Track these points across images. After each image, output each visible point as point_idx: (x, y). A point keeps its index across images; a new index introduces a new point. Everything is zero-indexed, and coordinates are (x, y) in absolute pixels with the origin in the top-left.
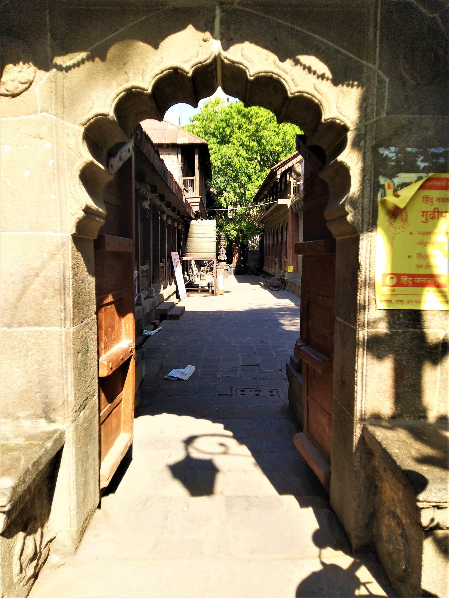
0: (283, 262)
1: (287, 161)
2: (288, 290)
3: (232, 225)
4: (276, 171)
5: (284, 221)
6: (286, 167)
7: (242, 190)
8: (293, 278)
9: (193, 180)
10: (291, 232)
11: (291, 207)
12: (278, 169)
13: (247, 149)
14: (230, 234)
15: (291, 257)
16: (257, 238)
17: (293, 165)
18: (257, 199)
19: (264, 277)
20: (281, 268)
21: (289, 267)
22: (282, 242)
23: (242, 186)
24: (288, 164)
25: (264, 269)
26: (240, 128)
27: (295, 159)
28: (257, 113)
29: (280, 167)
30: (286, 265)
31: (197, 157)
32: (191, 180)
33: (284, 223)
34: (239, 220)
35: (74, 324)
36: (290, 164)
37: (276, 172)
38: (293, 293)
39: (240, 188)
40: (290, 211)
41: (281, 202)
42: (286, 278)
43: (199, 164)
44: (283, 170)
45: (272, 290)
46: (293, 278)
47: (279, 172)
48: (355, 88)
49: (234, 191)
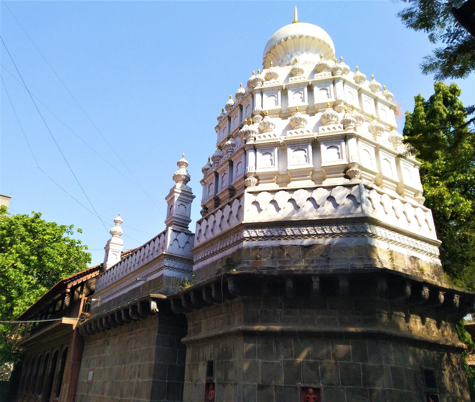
5: (62, 346)
6: (80, 281)
7: (9, 305)
10: (71, 360)
11: (77, 328)
12: (69, 282)
13: (27, 262)
15: (67, 395)
16: (11, 366)
18: (26, 316)
22: (30, 375)
24: (81, 279)
26: (23, 239)
27: (90, 275)
28: (44, 230)
29: (72, 280)
33: (62, 348)
36: (84, 279)
41: (66, 320)
44: (75, 283)
47: (69, 286)
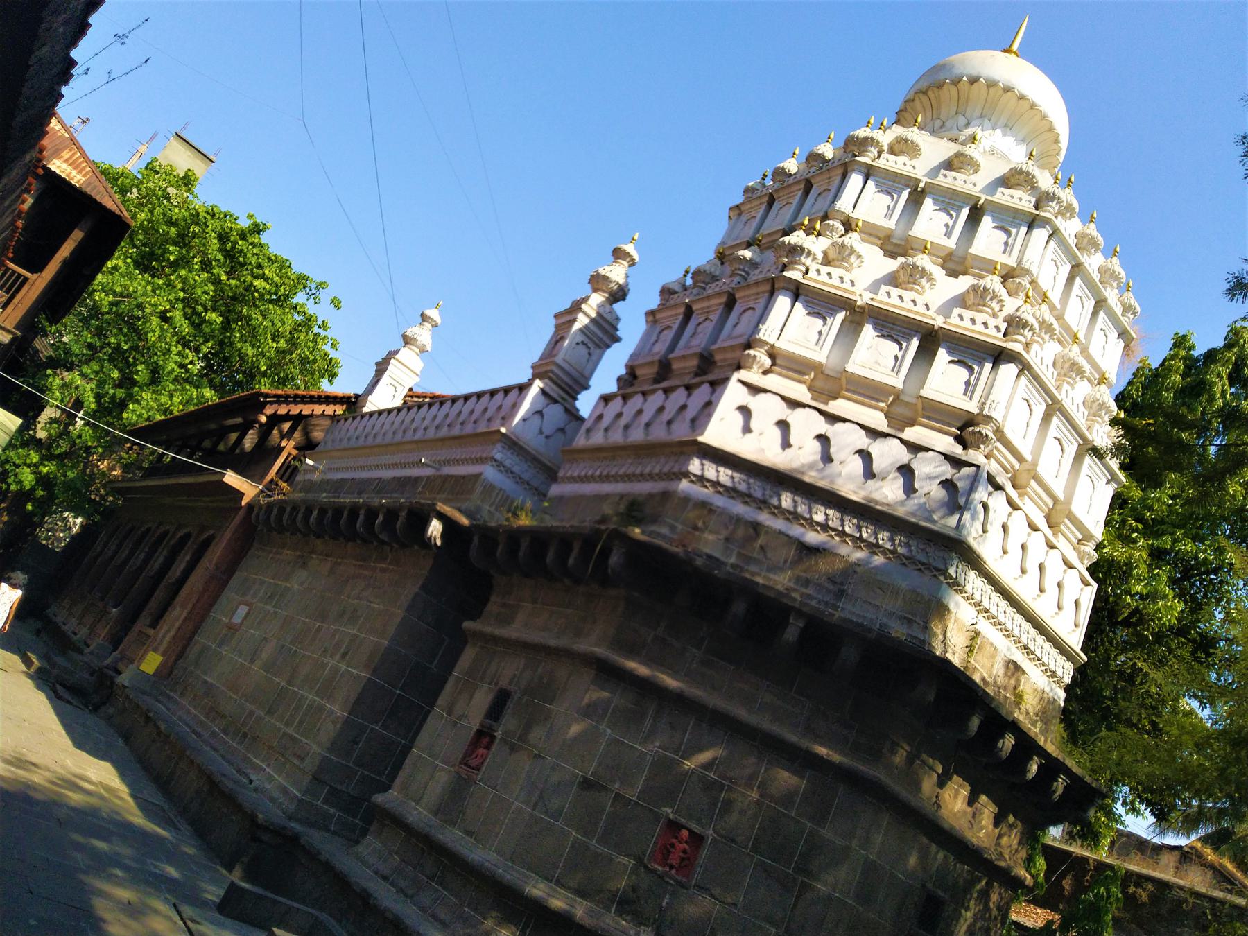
1: (303, 397)
2: (109, 719)
3: (35, 457)
4: (265, 403)
6: (295, 410)
7: (121, 393)
8: (144, 693)
9: (26, 279)
10: (212, 567)
11: (250, 506)
14: (16, 475)
15: (172, 633)
17: (311, 416)
19: (38, 633)
20: (116, 641)
21: (151, 655)
23: (127, 382)
24: (300, 406)
25: (50, 612)
26: (206, 266)
27: (323, 407)
28: (259, 266)
29: (280, 399)
30: (144, 643)
31: (77, 235)
32: (20, 275)
33: (178, 529)
34: (60, 455)
36: (306, 410)
38: (127, 738)
39: (120, 386)
40: (241, 513)
43: (72, 254)
44: (282, 410)
45: (59, 698)
46: (144, 693)
47: (269, 410)
49: (101, 384)
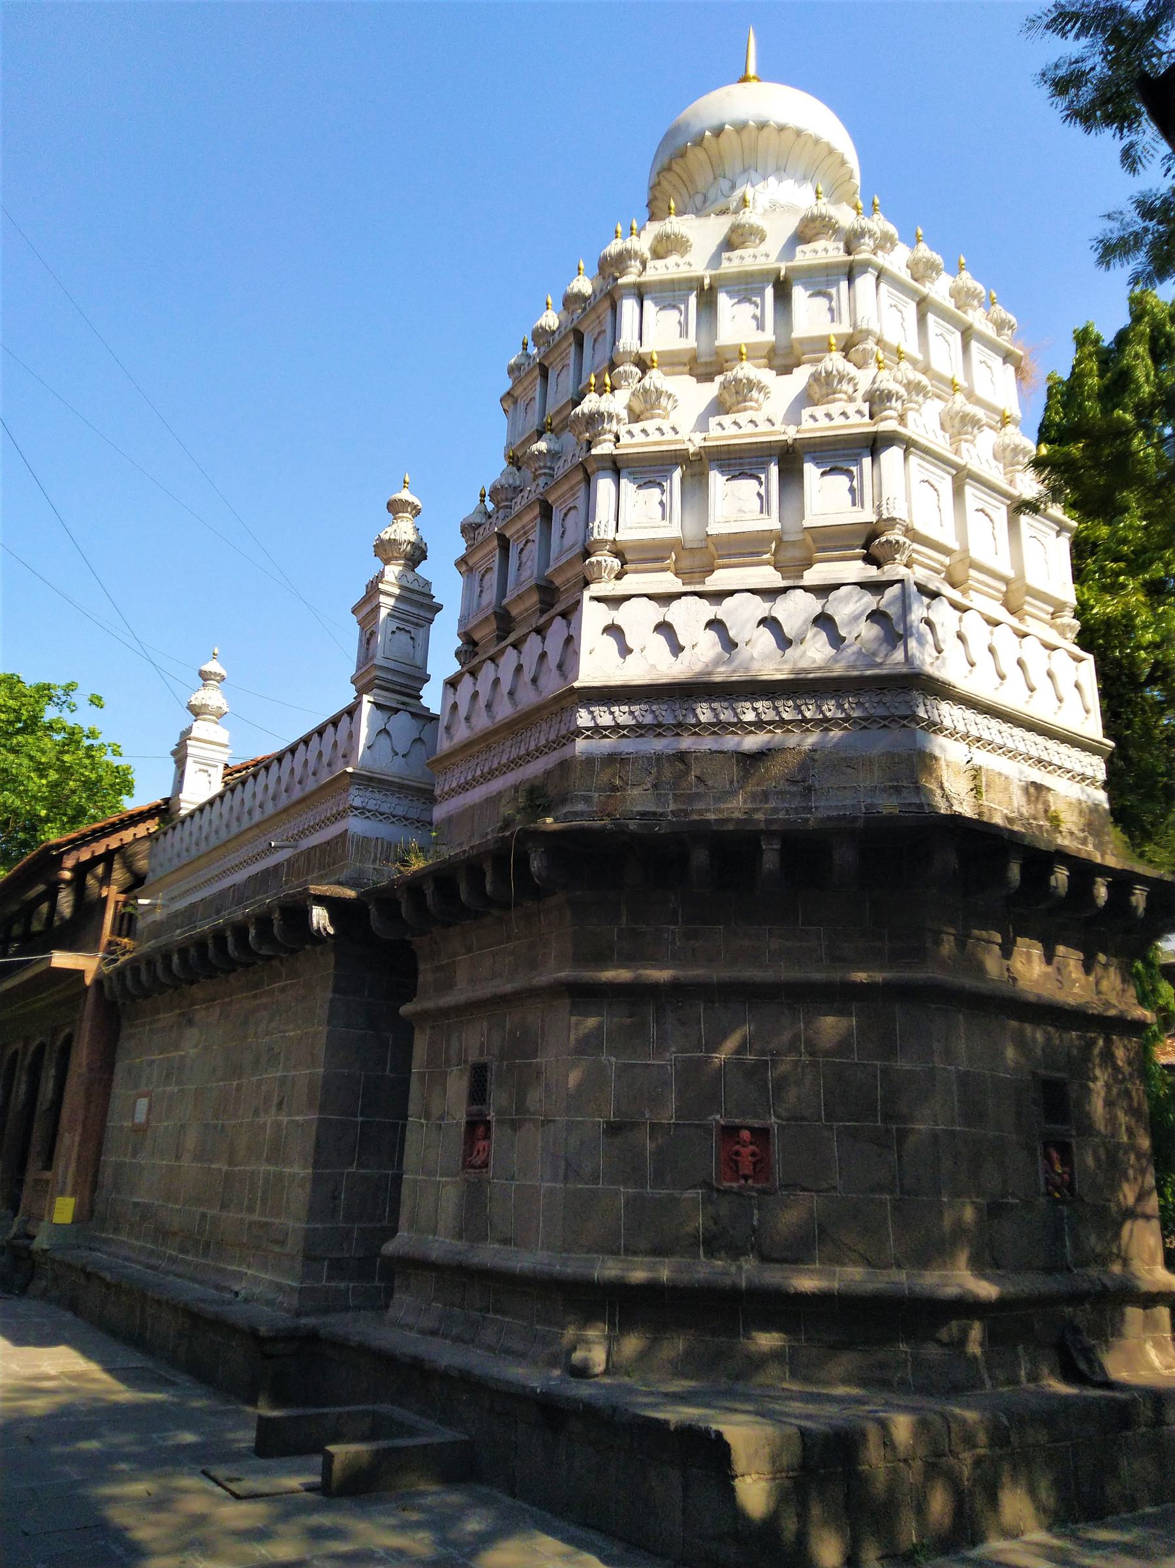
0: (29, 1177)
2: (44, 1295)
10: (84, 1070)
12: (68, 852)
24: (105, 841)
27: (132, 830)
29: (77, 844)
30: (46, 1191)
33: (26, 1046)
35: (334, 991)
37: (59, 859)
40: (91, 996)
41: (61, 960)
42: (41, 1242)
44: (85, 855)
47: (69, 862)
48: (1047, 86)
